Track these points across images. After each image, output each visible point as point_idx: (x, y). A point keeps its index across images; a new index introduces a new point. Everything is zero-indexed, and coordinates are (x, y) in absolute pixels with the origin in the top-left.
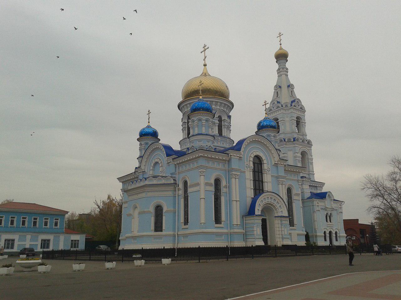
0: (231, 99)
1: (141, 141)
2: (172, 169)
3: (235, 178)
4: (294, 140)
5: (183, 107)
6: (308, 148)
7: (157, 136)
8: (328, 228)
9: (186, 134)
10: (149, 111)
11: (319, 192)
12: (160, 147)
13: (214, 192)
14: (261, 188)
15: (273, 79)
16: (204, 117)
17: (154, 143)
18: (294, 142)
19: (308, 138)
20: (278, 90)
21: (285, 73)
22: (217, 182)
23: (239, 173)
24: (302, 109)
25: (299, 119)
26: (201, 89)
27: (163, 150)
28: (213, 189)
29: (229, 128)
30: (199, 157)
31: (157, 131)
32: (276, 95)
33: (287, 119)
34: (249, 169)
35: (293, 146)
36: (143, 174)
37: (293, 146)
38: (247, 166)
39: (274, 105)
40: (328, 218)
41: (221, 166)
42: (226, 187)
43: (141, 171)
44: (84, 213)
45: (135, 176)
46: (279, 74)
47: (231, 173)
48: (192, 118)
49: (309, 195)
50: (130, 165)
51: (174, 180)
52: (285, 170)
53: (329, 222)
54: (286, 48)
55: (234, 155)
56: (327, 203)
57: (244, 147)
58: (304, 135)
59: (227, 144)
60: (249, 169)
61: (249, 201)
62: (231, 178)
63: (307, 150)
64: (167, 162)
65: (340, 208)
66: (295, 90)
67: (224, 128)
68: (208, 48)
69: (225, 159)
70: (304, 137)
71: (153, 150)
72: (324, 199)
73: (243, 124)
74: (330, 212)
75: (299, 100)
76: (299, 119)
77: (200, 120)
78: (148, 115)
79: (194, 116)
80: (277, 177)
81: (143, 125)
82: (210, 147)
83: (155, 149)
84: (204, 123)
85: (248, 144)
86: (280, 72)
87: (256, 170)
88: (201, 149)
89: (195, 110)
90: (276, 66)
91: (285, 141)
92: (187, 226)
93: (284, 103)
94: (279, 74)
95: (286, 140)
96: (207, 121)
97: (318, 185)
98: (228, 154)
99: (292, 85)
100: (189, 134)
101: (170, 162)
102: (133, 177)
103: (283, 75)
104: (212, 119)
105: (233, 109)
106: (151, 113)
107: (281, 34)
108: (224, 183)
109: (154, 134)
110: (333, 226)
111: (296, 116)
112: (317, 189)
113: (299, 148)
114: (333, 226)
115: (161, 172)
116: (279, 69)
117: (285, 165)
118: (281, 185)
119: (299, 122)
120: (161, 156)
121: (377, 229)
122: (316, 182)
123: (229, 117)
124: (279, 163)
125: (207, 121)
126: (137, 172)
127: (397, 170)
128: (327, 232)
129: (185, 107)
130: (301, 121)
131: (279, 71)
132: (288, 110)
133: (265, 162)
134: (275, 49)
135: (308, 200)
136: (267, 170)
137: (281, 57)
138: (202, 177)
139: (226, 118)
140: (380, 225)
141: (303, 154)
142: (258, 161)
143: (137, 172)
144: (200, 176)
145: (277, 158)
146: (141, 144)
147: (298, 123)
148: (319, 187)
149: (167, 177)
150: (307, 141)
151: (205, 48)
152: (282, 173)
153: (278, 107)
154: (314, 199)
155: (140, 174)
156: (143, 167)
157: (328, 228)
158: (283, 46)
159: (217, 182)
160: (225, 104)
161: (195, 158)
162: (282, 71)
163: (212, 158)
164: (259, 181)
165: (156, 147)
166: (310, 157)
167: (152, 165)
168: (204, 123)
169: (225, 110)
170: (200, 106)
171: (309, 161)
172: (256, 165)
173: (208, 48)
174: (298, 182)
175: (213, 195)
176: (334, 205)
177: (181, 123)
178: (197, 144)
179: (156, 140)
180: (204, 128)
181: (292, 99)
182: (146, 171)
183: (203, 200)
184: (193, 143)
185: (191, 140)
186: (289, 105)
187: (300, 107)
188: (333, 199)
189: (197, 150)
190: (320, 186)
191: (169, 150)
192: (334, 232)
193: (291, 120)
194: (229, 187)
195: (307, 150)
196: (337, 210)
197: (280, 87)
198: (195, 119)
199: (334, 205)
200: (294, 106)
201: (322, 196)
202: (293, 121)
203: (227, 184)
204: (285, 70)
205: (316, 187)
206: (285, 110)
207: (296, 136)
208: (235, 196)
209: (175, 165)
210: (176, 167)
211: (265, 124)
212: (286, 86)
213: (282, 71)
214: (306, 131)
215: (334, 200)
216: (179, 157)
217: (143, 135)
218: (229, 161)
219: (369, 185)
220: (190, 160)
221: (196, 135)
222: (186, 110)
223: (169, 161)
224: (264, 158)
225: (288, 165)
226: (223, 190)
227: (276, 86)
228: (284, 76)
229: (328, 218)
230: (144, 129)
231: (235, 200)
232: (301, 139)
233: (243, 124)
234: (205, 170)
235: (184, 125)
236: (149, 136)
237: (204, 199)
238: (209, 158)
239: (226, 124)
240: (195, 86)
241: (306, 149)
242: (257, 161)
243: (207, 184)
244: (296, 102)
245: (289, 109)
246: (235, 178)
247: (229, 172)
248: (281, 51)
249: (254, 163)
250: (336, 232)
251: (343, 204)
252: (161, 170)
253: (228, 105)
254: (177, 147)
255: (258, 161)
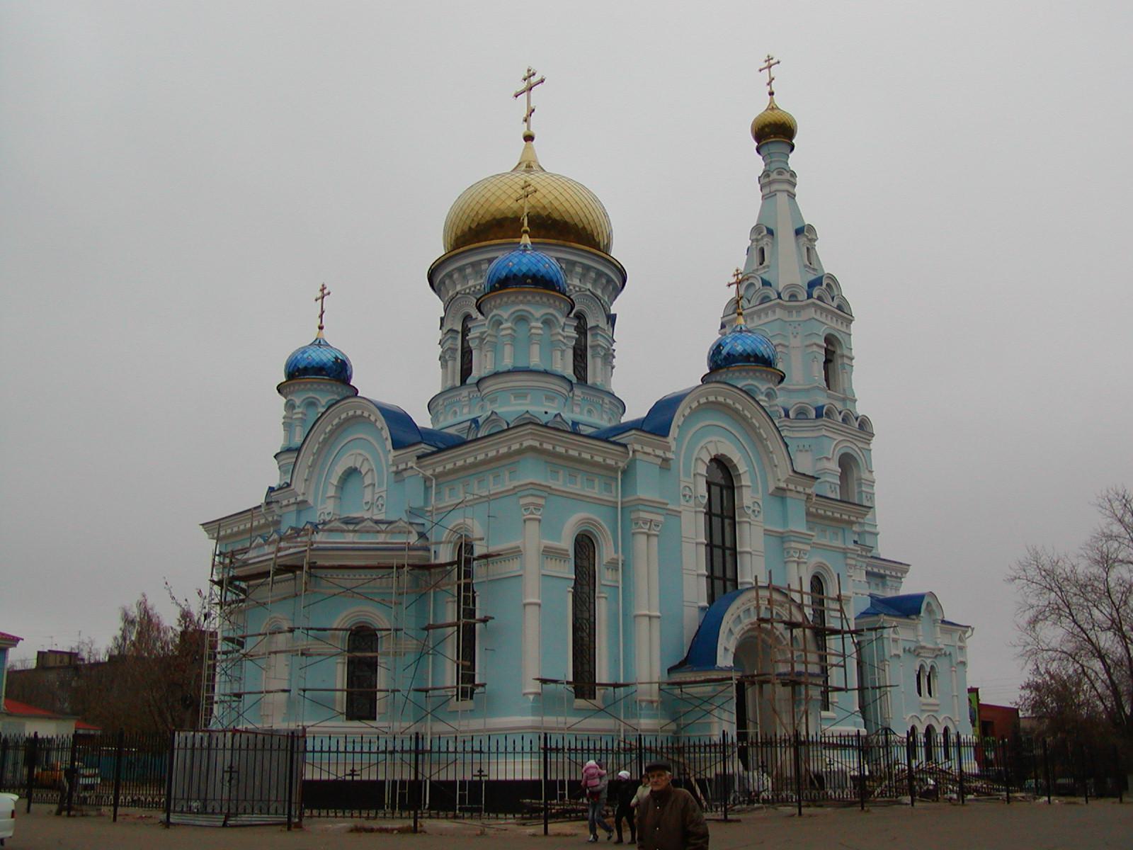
0: (617, 252)
1: (291, 393)
2: (413, 493)
3: (648, 536)
4: (819, 415)
5: (450, 275)
6: (860, 445)
7: (349, 378)
8: (924, 717)
9: (454, 372)
10: (322, 290)
11: (890, 594)
12: (366, 414)
13: (572, 583)
14: (729, 574)
15: (748, 205)
16: (538, 309)
17: (338, 402)
18: (819, 422)
19: (860, 409)
20: (762, 243)
21: (786, 187)
22: (585, 545)
23: (661, 518)
24: (843, 312)
25: (833, 345)
26: (526, 211)
27: (382, 423)
28: (567, 570)
29: (608, 356)
30: (520, 452)
31: (347, 358)
32: (756, 259)
33: (794, 342)
34: (692, 502)
35: (815, 434)
36: (299, 512)
37: (815, 434)
38: (687, 492)
39: (752, 291)
40: (925, 680)
41: (596, 490)
42: (613, 565)
43: (292, 500)
44: (54, 648)
45: (270, 519)
46: (767, 191)
47: (633, 516)
48: (495, 312)
49: (866, 604)
50: (249, 479)
51: (422, 535)
52: (808, 514)
53: (925, 697)
54: (789, 106)
55: (649, 450)
56: (920, 632)
57: (680, 424)
58: (850, 399)
59: (605, 416)
60: (692, 502)
61: (691, 621)
62: (633, 534)
63: (857, 449)
64: (394, 469)
65: (961, 648)
66: (819, 247)
67: (593, 357)
68: (542, 81)
69: (613, 463)
70: (849, 404)
71: (339, 425)
72: (914, 617)
73: (657, 347)
74: (930, 660)
75: (831, 277)
76: (833, 345)
77: (522, 319)
78: (320, 301)
79: (500, 304)
80: (782, 538)
81: (294, 339)
82: (558, 419)
83: (347, 420)
84: (540, 332)
85: (694, 412)
86: (770, 183)
87: (716, 509)
88: (528, 421)
89: (506, 283)
90: (758, 164)
91: (787, 415)
92: (469, 704)
93: (787, 287)
94: (767, 191)
95: (791, 414)
96: (549, 324)
97: (888, 572)
98: (625, 446)
99: (811, 228)
100: (466, 371)
101: (405, 469)
102: (262, 521)
103: (778, 194)
104: (563, 316)
105: (625, 288)
106: (329, 293)
107: (772, 62)
108: (606, 552)
109: (339, 372)
110: (936, 708)
111: (823, 331)
112: (884, 585)
113: (835, 444)
114: (936, 708)
115: (370, 505)
116: (766, 174)
117: (809, 496)
118: (796, 565)
119: (833, 355)
120: (371, 453)
121: (982, 713)
122: (884, 560)
123: (612, 319)
124: (791, 487)
125: (548, 322)
126: (278, 502)
127: (1117, 529)
128: (921, 730)
129: (447, 282)
130: (839, 352)
131: (767, 180)
132: (800, 309)
133: (745, 481)
134: (756, 108)
135: (863, 620)
136: (750, 512)
137: (774, 134)
138: (532, 528)
139: (603, 323)
140: (1037, 705)
141: (847, 463)
142: (723, 476)
143: (278, 502)
144: (525, 521)
145: (784, 472)
146: (290, 406)
147: (829, 357)
148: (892, 576)
149: (395, 522)
150: (857, 419)
151: (531, 82)
152: (798, 524)
153: (765, 299)
154: (885, 618)
155: (285, 510)
156: (299, 486)
157: (924, 717)
158: (779, 101)
159: (585, 545)
160: (600, 274)
161: (508, 455)
162: (777, 181)
163: (581, 461)
164: (723, 547)
165: (351, 413)
166: (865, 475)
167: (335, 480)
168: (540, 332)
169: (599, 293)
170: (524, 269)
171: (864, 489)
172: (715, 490)
173: (542, 81)
174: (846, 558)
175: (570, 596)
176: (943, 641)
177: (438, 335)
178: (510, 409)
179: (346, 392)
180: (535, 349)
181: (812, 277)
182: (311, 501)
183: (532, 613)
184: (493, 401)
185: (483, 393)
186: (803, 296)
187: (835, 304)
188: (940, 618)
189: (511, 426)
190: (894, 574)
191: (398, 421)
192: (939, 730)
193: (807, 346)
194: (624, 567)
195: (857, 449)
196: (950, 654)
197: (771, 232)
198: (505, 313)
199: (943, 641)
200: (819, 298)
201: (909, 607)
202: (815, 348)
203: (616, 552)
204: (787, 176)
205: (883, 577)
206: (789, 310)
207: (822, 399)
208: (647, 601)
209: (426, 479)
210: (427, 489)
211: (739, 348)
212: (793, 234)
213: (777, 181)
214: (853, 387)
215: (943, 622)
216: (440, 450)
217: (301, 373)
218: (624, 472)
219: (1032, 572)
220: (498, 458)
221: (509, 372)
222: (459, 288)
223: (402, 467)
224: (742, 468)
225: (817, 495)
226: (604, 577)
227: (757, 229)
228: (782, 198)
229: (925, 680)
230: (304, 350)
231: (647, 612)
232: (840, 413)
233: (657, 347)
234: (542, 502)
235: (450, 341)
236: (318, 377)
237: (539, 605)
238: (559, 456)
239: (602, 342)
240: (506, 201)
241: (854, 448)
242: (719, 477)
243: (550, 553)
244: (824, 285)
245: (803, 307)
246: (648, 536)
247: (626, 512)
248: (773, 117)
249: (709, 484)
250: (946, 730)
251: (967, 635)
252: (368, 496)
253: (610, 277)
254: (423, 420)
255: (723, 476)
